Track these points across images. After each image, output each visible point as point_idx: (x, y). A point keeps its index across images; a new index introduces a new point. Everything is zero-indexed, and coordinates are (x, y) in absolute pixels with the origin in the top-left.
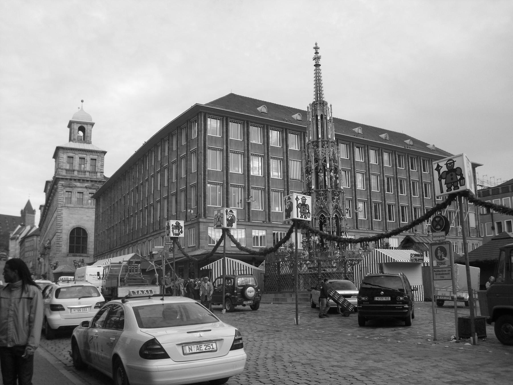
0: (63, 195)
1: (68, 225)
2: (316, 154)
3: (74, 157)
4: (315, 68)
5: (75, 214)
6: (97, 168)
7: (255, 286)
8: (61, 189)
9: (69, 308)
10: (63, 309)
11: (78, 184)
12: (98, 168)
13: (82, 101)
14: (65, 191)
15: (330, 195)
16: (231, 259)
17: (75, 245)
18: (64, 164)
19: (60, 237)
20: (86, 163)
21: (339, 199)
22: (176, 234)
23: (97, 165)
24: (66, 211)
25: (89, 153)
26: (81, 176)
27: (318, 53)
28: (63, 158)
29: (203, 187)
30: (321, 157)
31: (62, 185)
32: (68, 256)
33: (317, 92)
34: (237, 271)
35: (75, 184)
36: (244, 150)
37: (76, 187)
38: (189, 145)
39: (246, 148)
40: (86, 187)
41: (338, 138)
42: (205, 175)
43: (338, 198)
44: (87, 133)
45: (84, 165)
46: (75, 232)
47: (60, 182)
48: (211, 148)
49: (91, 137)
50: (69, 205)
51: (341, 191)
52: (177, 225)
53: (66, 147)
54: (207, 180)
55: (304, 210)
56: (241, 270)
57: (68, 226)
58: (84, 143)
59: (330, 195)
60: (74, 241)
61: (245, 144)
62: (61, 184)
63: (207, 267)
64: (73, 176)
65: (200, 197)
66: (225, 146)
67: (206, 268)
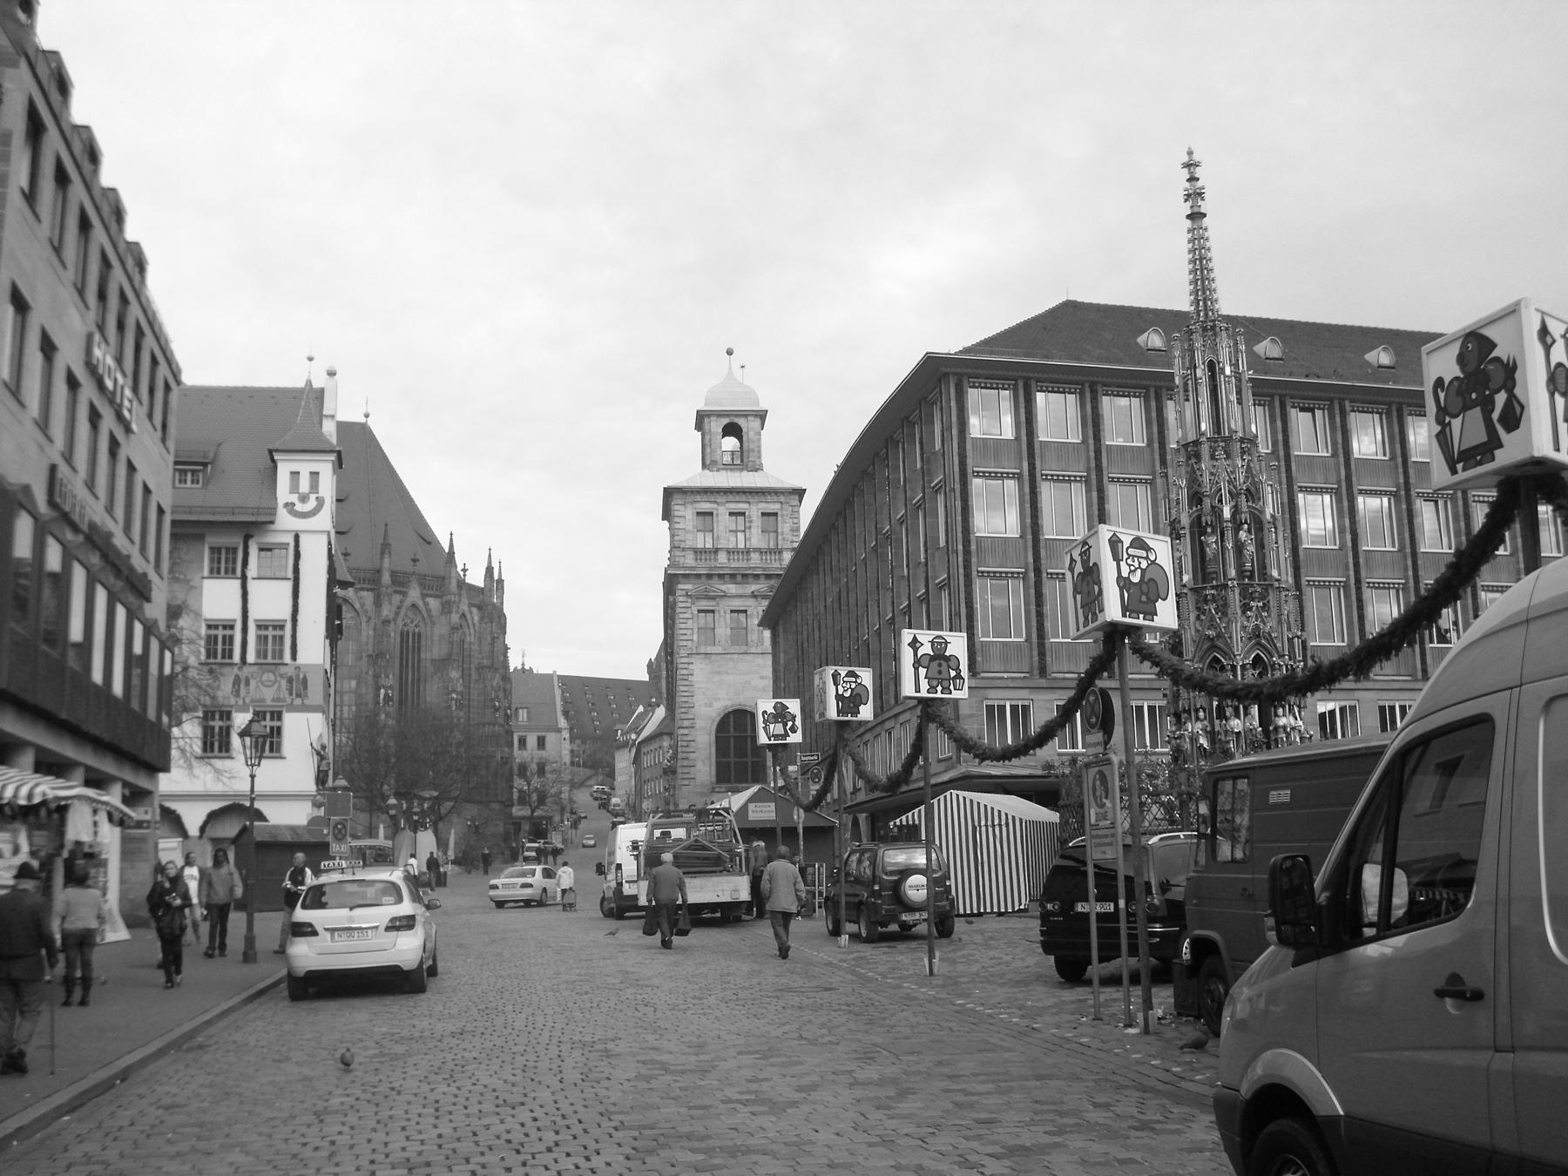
0: (690, 621)
1: (711, 705)
2: (1194, 481)
3: (715, 513)
4: (1188, 223)
5: (727, 673)
6: (780, 537)
7: (935, 871)
8: (684, 605)
9: (326, 929)
10: (315, 933)
11: (732, 588)
12: (784, 539)
13: (730, 352)
14: (695, 609)
15: (1235, 598)
16: (959, 792)
17: (732, 759)
18: (689, 536)
19: (689, 738)
20: (750, 528)
21: (1266, 607)
22: (776, 737)
23: (779, 530)
24: (703, 666)
25: (757, 498)
26: (738, 564)
27: (1198, 179)
28: (684, 517)
29: (962, 588)
30: (1207, 488)
31: (687, 595)
32: (713, 791)
33: (1197, 294)
34: (983, 829)
35: (723, 587)
36: (1088, 470)
37: (725, 596)
38: (929, 469)
39: (1093, 464)
40: (754, 596)
41: (1401, 400)
42: (967, 552)
43: (1261, 604)
44: (748, 441)
45: (744, 531)
46: (732, 724)
47: (680, 586)
48: (984, 472)
49: (759, 452)
50: (709, 649)
51: (1272, 585)
52: (779, 711)
53: (691, 488)
54: (974, 568)
55: (940, 672)
56: (993, 826)
57: (708, 709)
58: (742, 470)
59: (1235, 598)
60: (729, 749)
61: (1088, 451)
62: (684, 593)
63: (907, 821)
64: (716, 567)
65: (957, 618)
66: (1025, 465)
67: (904, 823)
